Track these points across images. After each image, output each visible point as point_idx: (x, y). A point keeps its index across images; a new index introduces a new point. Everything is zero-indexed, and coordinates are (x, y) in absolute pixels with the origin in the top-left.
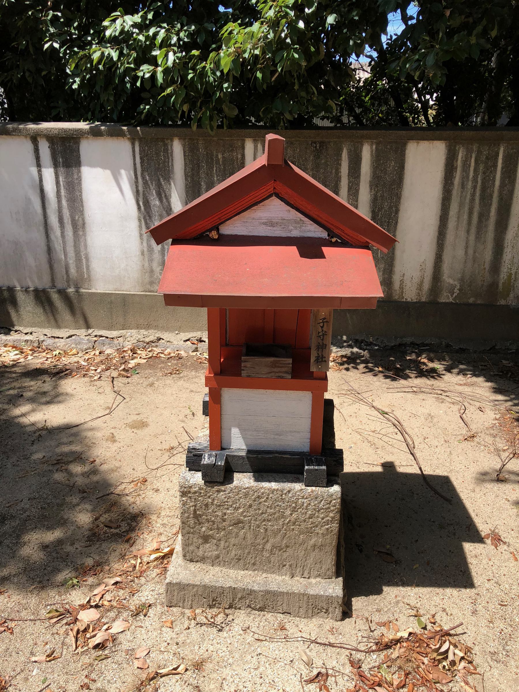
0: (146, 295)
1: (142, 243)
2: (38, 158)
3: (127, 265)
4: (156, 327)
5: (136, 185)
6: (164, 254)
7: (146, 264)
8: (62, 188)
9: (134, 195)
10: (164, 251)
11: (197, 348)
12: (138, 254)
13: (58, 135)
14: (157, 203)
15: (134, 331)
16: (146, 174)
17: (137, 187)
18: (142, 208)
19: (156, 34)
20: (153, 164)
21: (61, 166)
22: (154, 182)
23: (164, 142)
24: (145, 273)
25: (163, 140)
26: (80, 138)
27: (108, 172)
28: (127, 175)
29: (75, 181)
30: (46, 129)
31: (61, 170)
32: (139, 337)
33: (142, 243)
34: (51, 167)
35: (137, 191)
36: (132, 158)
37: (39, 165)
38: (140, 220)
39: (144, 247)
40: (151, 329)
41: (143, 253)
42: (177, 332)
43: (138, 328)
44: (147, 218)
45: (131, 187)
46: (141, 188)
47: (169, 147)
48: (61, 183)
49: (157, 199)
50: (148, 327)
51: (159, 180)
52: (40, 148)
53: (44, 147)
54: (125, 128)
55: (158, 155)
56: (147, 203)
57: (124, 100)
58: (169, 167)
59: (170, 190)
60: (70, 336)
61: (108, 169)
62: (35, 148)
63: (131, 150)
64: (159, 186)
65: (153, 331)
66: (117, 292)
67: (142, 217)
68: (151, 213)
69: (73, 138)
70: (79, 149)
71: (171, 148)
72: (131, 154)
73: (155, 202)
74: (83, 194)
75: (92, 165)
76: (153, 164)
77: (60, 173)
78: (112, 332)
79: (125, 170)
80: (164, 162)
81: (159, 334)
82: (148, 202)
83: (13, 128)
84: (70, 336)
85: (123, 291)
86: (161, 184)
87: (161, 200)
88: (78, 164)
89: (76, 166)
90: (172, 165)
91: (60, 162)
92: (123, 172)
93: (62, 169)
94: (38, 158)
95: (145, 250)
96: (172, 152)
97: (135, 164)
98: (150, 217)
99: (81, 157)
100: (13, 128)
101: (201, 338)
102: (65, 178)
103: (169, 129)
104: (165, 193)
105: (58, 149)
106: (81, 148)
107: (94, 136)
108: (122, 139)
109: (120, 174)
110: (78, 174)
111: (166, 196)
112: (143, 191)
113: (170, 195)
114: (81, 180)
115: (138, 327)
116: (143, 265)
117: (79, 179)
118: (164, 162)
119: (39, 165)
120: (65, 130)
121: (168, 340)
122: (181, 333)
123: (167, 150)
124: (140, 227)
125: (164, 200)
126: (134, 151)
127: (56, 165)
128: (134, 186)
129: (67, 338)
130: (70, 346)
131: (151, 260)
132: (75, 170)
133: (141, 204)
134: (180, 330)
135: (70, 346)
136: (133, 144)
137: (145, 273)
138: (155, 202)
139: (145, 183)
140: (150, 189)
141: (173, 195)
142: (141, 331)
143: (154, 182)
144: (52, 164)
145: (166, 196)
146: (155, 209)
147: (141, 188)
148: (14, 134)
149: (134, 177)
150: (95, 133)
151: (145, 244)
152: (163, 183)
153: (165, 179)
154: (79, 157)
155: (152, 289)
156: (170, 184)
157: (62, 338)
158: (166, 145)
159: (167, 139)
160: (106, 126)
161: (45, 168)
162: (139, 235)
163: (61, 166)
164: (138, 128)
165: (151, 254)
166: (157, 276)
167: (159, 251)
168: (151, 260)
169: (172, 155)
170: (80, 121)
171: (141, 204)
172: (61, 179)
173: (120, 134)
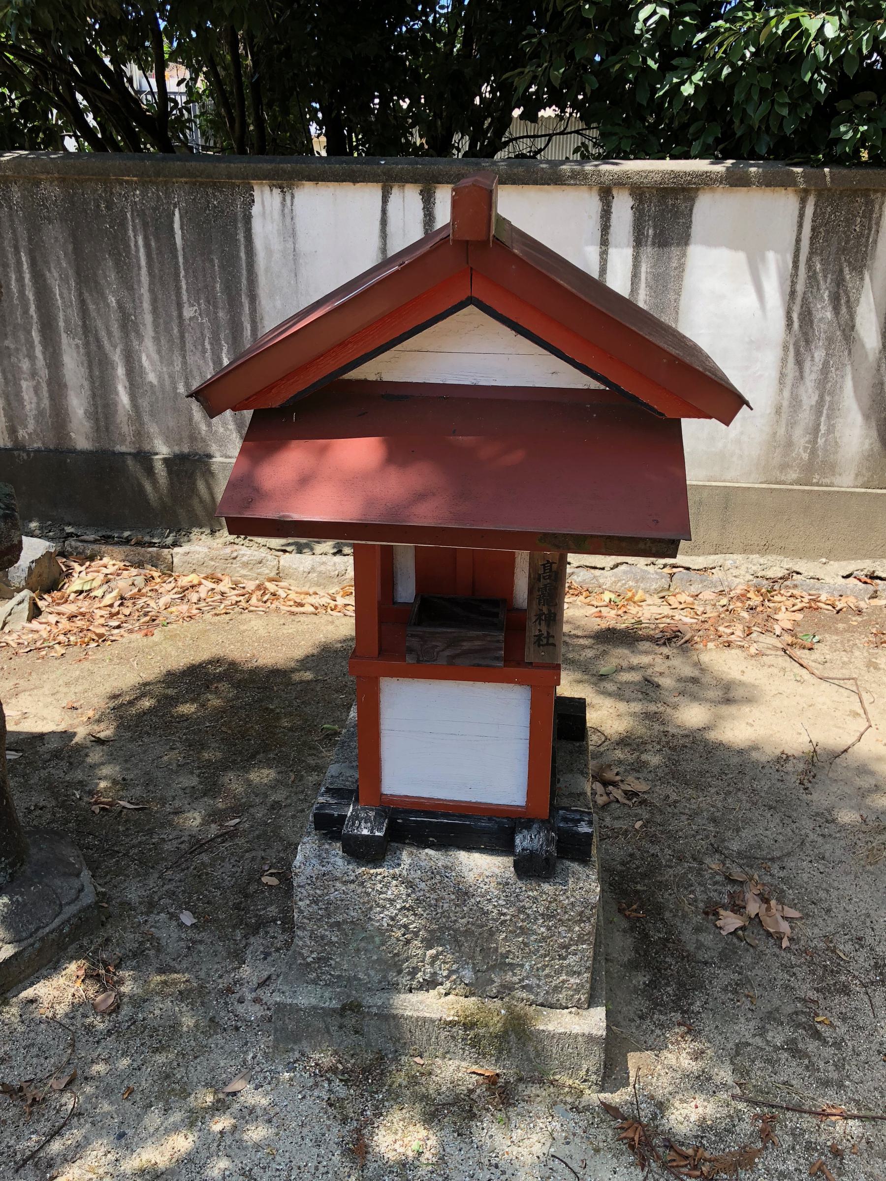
0: (772, 490)
1: (781, 390)
2: (605, 228)
3: (742, 433)
4: (782, 551)
5: (792, 282)
6: (821, 412)
7: (782, 431)
8: (643, 285)
9: (783, 299)
10: (823, 406)
11: (876, 592)
12: (768, 411)
13: (661, 184)
14: (829, 315)
15: (739, 558)
16: (817, 259)
17: (793, 284)
18: (796, 325)
19: (171, 43)
20: (835, 240)
21: (649, 243)
22: (829, 276)
23: (868, 196)
24: (775, 447)
25: (866, 193)
26: (698, 189)
27: (741, 257)
28: (777, 261)
29: (672, 273)
30: (638, 173)
31: (648, 251)
32: (754, 568)
33: (781, 390)
34: (628, 246)
35: (793, 293)
36: (795, 228)
37: (604, 242)
38: (786, 348)
39: (783, 399)
40: (772, 552)
41: (778, 411)
42: (824, 560)
43: (745, 551)
44: (802, 343)
45: (782, 284)
46: (800, 287)
47: (877, 207)
48: (643, 276)
49: (830, 308)
50: (765, 549)
51: (841, 271)
52: (613, 210)
53: (623, 207)
54: (799, 170)
55: (849, 222)
56: (807, 317)
57: (807, 115)
58: (866, 247)
59: (859, 291)
60: (616, 566)
61: (742, 250)
62: (603, 210)
63: (797, 213)
64: (840, 281)
65: (775, 557)
66: (714, 484)
67: (792, 342)
68: (810, 334)
69: (684, 190)
70: (691, 210)
71: (881, 208)
72: (795, 219)
73: (824, 313)
74: (682, 298)
75: (711, 243)
76: (835, 240)
77: (643, 258)
78: (693, 557)
79: (776, 252)
80: (860, 236)
81: (789, 564)
82: (810, 313)
83: (572, 171)
84: (616, 566)
85: (724, 481)
86: (843, 280)
87: (836, 309)
88: (685, 239)
89: (678, 245)
90: (875, 242)
91: (648, 236)
92: (771, 256)
93: (649, 249)
94: (605, 228)
95: (785, 403)
96: (881, 215)
97: (798, 241)
98: (808, 342)
99: (693, 227)
100: (572, 171)
101: (874, 572)
102: (651, 267)
103: (862, 171)
104: (848, 297)
105: (649, 211)
106: (695, 211)
107: (731, 186)
108: (784, 191)
109: (763, 259)
110: (679, 259)
111: (848, 301)
112: (805, 293)
113: (858, 300)
114: (683, 270)
115: (746, 550)
116: (775, 433)
117: (681, 268)
118: (860, 236)
119: (604, 242)
120: (676, 175)
121: (811, 574)
122: (832, 562)
123: (871, 212)
124: (784, 361)
125: (844, 310)
126: (801, 216)
127: (638, 242)
128: (789, 283)
129: (612, 569)
130: (625, 584)
131: (792, 424)
132: (675, 251)
133: (795, 316)
134: (831, 555)
135: (625, 584)
136: (803, 202)
137: (775, 447)
138: (824, 313)
139: (812, 277)
140: (819, 289)
141: (863, 300)
142: (751, 556)
143: (829, 276)
144: (632, 239)
145: (848, 301)
146: (822, 326)
147: (800, 287)
148: (572, 182)
149: (791, 265)
150: (736, 180)
151: (786, 393)
152: (848, 277)
153: (853, 269)
154: (689, 227)
155: (783, 478)
156: (862, 279)
157: (603, 569)
158: (870, 203)
159: (876, 191)
160: (758, 166)
161: (616, 247)
162: (778, 375)
163: (649, 243)
164: (826, 170)
165: (795, 411)
166: (799, 454)
167: (812, 406)
168: (792, 424)
169: (878, 224)
170: (664, 158)
171: (795, 316)
172: (644, 268)
173: (786, 182)
